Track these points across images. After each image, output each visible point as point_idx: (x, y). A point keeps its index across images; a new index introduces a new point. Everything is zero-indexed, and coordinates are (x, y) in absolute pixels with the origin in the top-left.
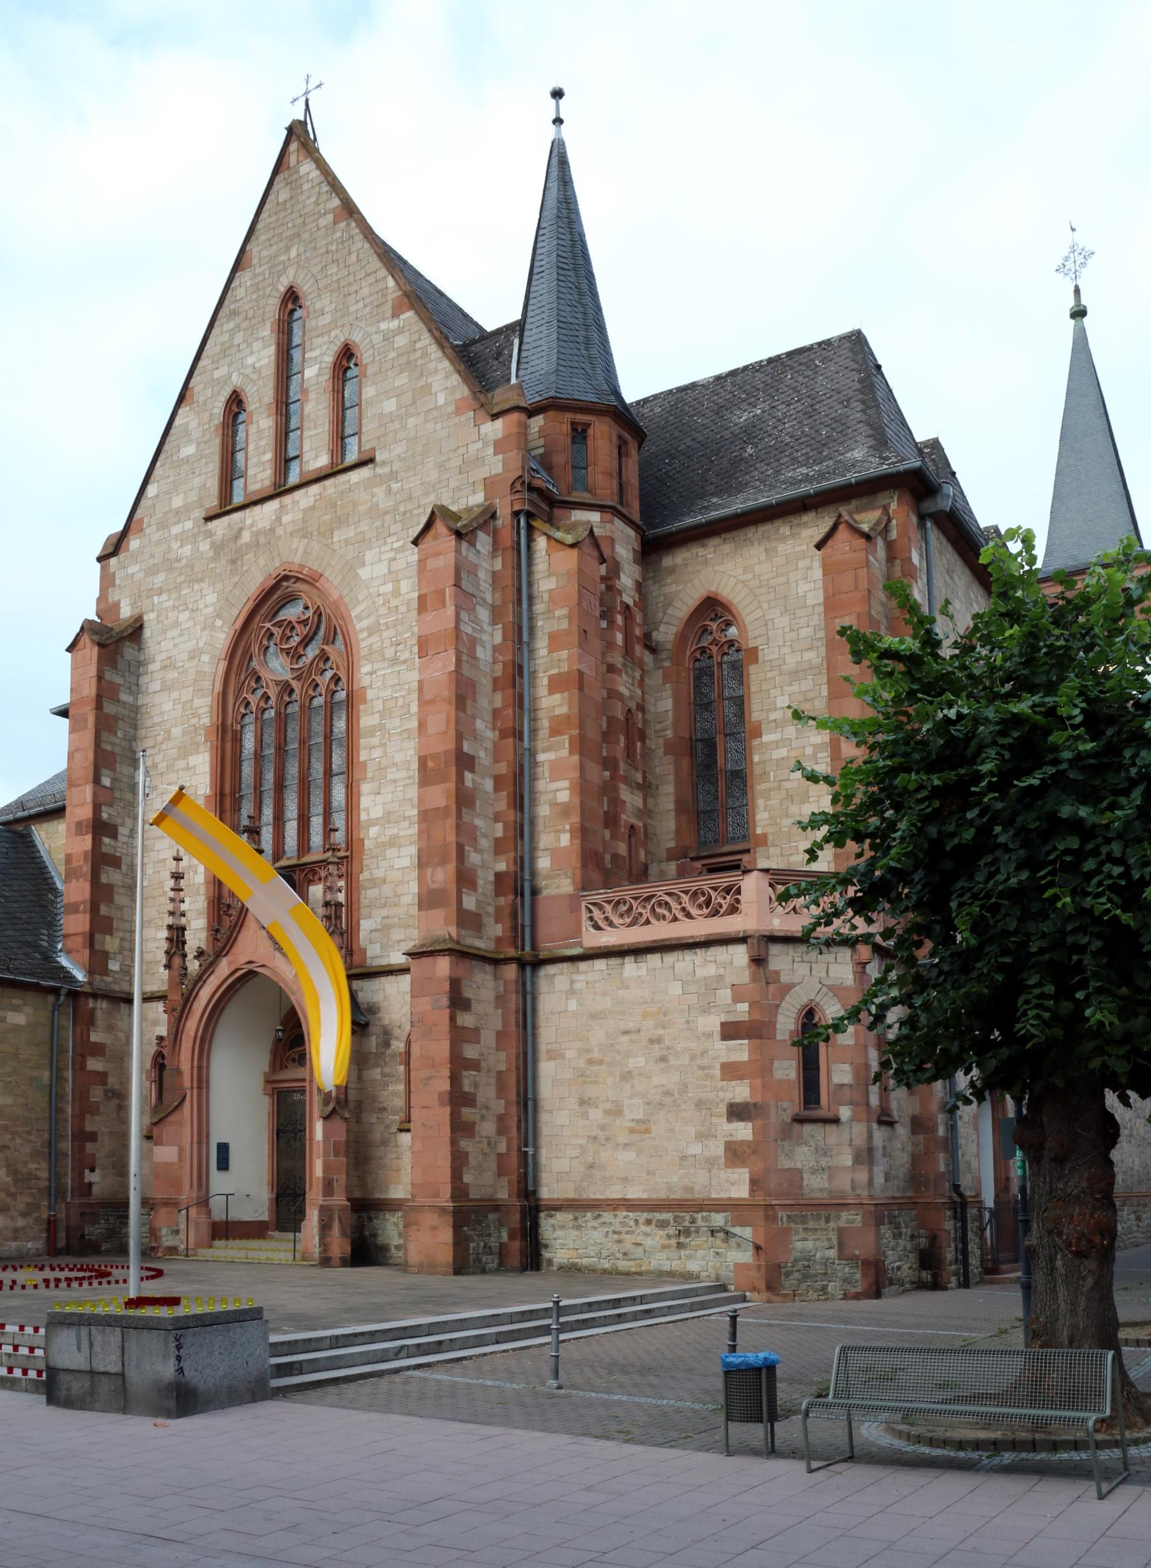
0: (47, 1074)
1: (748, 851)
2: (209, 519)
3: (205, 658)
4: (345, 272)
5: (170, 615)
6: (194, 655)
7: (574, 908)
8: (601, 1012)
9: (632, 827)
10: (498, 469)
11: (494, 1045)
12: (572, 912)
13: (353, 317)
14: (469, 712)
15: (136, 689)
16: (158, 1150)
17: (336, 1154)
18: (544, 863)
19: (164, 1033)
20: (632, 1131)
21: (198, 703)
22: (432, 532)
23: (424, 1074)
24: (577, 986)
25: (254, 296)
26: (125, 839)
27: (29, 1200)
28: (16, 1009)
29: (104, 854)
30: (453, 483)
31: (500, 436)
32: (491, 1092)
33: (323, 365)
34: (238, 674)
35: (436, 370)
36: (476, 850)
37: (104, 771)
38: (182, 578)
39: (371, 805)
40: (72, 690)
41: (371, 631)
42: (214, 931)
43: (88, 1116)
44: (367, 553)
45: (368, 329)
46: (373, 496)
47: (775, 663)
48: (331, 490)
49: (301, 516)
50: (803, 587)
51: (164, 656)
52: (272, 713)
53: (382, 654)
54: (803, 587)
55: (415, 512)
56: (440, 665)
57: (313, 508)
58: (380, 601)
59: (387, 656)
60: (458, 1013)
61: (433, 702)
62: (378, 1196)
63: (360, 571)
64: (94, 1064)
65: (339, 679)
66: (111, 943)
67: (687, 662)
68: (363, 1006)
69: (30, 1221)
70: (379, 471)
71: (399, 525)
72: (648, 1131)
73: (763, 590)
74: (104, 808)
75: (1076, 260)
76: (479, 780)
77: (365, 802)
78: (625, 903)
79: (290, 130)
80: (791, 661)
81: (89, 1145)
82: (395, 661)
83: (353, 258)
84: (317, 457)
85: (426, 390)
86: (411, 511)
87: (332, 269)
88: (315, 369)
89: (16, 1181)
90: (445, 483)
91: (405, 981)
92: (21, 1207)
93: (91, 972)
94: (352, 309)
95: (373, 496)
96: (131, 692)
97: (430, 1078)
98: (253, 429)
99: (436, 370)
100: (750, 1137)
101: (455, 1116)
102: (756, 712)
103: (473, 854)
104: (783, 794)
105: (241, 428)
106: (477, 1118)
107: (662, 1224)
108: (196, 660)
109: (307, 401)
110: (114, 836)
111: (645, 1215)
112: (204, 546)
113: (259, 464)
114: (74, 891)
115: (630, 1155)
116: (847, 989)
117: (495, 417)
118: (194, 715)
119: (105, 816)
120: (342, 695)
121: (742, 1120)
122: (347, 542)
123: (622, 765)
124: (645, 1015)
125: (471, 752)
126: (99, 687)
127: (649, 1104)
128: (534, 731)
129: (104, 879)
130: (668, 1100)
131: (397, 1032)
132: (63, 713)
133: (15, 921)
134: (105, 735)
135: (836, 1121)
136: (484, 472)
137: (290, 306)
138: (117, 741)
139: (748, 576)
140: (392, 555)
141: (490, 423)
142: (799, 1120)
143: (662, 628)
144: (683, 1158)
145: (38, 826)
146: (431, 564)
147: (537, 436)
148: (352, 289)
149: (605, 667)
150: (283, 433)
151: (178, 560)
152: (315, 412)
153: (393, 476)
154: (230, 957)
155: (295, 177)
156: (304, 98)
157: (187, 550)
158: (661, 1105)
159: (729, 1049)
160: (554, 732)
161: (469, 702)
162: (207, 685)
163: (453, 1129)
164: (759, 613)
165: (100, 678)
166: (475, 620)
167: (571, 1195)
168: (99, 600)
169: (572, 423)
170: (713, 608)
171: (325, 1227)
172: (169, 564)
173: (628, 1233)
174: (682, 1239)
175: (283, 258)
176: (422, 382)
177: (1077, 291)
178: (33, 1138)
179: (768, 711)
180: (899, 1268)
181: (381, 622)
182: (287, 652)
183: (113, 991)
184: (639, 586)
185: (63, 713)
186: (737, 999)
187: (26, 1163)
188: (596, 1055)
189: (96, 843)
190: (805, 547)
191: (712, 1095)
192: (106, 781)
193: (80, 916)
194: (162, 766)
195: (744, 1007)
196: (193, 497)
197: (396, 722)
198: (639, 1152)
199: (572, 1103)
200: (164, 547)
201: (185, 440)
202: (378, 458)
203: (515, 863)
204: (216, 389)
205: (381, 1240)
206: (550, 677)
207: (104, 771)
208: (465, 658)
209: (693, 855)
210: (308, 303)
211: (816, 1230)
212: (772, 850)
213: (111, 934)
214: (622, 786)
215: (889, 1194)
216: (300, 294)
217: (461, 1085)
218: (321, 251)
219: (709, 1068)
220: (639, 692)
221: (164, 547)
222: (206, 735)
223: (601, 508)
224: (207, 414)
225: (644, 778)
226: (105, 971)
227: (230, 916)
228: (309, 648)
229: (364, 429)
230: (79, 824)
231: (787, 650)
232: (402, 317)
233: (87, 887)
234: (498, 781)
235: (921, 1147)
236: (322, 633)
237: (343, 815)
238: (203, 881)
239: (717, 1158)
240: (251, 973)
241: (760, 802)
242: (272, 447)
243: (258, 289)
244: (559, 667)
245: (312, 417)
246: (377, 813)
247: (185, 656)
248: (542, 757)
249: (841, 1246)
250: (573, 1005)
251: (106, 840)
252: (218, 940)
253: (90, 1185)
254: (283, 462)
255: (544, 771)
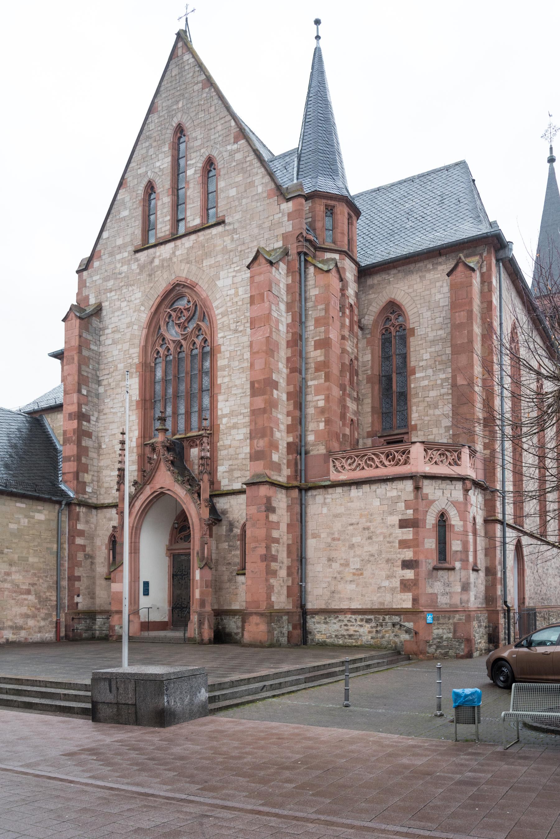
0: (55, 546)
1: (407, 433)
2: (136, 252)
3: (136, 327)
4: (208, 117)
5: (116, 303)
6: (130, 325)
7: (326, 461)
8: (339, 514)
9: (352, 420)
10: (290, 229)
11: (286, 531)
12: (325, 463)
13: (212, 142)
14: (276, 358)
15: (99, 343)
16: (113, 585)
17: (207, 587)
18: (311, 438)
19: (116, 525)
20: (354, 574)
21: (132, 351)
22: (258, 262)
23: (253, 545)
24: (327, 501)
25: (159, 128)
26: (94, 423)
27: (47, 612)
28: (39, 512)
29: (83, 430)
30: (266, 236)
31: (291, 210)
32: (285, 554)
33: (197, 168)
34: (153, 336)
35: (257, 173)
36: (279, 431)
37: (83, 387)
38: (123, 284)
39: (224, 406)
40: (65, 342)
41: (224, 314)
42: (142, 471)
43: (76, 568)
44: (221, 273)
45: (221, 149)
46: (224, 242)
47: (423, 336)
48: (202, 238)
49: (186, 251)
50: (438, 296)
51: (113, 325)
52: (171, 357)
53: (229, 327)
54: (438, 296)
55: (246, 251)
56: (261, 333)
57: (192, 247)
58: (228, 299)
59: (232, 328)
60: (270, 514)
61: (258, 352)
62: (226, 608)
63: (217, 282)
64: (79, 541)
65: (206, 340)
66: (87, 478)
67: (379, 336)
68: (219, 511)
69: (47, 622)
70: (227, 228)
71: (238, 258)
72: (362, 574)
73: (417, 298)
74: (83, 406)
75: (550, 133)
76: (280, 394)
77: (220, 405)
78: (351, 458)
79: (178, 34)
80: (431, 335)
81: (76, 583)
82: (236, 331)
83: (213, 109)
84: (194, 219)
85: (251, 184)
86: (244, 250)
87: (201, 115)
88: (193, 171)
89: (40, 602)
90: (262, 236)
91: (243, 497)
92: (42, 615)
93: (77, 492)
94: (212, 137)
95: (224, 242)
96: (96, 345)
97: (256, 547)
98: (159, 203)
99: (257, 173)
100: (413, 578)
101: (268, 566)
102: (413, 362)
103: (277, 433)
104: (426, 404)
105: (153, 202)
106: (278, 568)
107: (368, 621)
108: (131, 328)
109: (189, 188)
110: (89, 421)
111: (360, 617)
112: (134, 266)
113: (164, 222)
114: (66, 450)
115: (353, 586)
116: (460, 503)
117: (288, 200)
118: (130, 358)
119: (84, 410)
120: (208, 349)
121: (409, 569)
122: (210, 266)
123: (348, 388)
124: (361, 516)
125: (276, 380)
126: (80, 341)
127: (362, 560)
128: (306, 369)
129: (84, 444)
130: (372, 559)
131: (236, 524)
132: (58, 355)
133: (37, 465)
134: (83, 367)
135: (453, 569)
136: (282, 230)
137: (179, 135)
138: (90, 371)
139: (411, 290)
140: (234, 274)
141: (285, 204)
142: (436, 569)
143: (366, 317)
144: (379, 588)
145: (46, 415)
146: (257, 279)
147: (308, 211)
148: (212, 126)
149: (340, 338)
150: (177, 204)
151: (120, 274)
152: (193, 194)
153: (235, 231)
154: (151, 485)
155: (181, 62)
156: (185, 18)
157: (125, 268)
158: (369, 561)
159: (403, 533)
160: (317, 370)
161: (276, 353)
162: (137, 341)
163: (267, 574)
164: (415, 310)
165: (80, 336)
166: (278, 310)
167: (323, 607)
168: (78, 294)
169: (326, 205)
170: (393, 308)
171: (201, 623)
172: (115, 275)
173: (351, 626)
174: (379, 629)
175: (175, 107)
176: (249, 180)
177: (551, 148)
178: (48, 579)
179: (419, 361)
180: (480, 642)
181: (229, 310)
182: (179, 325)
183: (88, 503)
184: (357, 295)
185: (58, 355)
186: (407, 508)
187: (45, 592)
188: (336, 536)
189: (80, 425)
190: (439, 275)
191: (394, 556)
192: (84, 392)
193: (71, 463)
194: (113, 385)
195: (410, 512)
196: (128, 239)
197: (236, 363)
198: (357, 585)
199: (324, 560)
200: (113, 266)
201: (123, 207)
202: (227, 221)
203: (297, 438)
204: (139, 180)
205: (227, 630)
206: (315, 341)
207: (83, 387)
208: (274, 330)
209: (379, 435)
210: (189, 133)
211: (443, 624)
212: (419, 432)
213: (87, 473)
214: (348, 399)
215: (476, 606)
216: (185, 128)
217: (271, 551)
218: (195, 104)
219: (393, 542)
220: (356, 350)
221: (113, 266)
222: (136, 368)
223: (340, 252)
224: (135, 194)
225: (358, 395)
226: (85, 492)
227: (151, 464)
228: (190, 323)
229: (219, 205)
230: (70, 414)
231: (430, 329)
232: (239, 143)
233: (75, 448)
234: (289, 394)
235: (490, 582)
236: (197, 313)
237: (208, 412)
238: (135, 445)
239: (396, 588)
240: (162, 493)
241: (414, 408)
242: (170, 213)
243: (161, 125)
244: (319, 336)
245: (191, 197)
246: (226, 411)
247: (124, 326)
248: (310, 383)
249: (455, 632)
250: (325, 510)
251: (85, 423)
252: (144, 476)
253: (77, 603)
254: (176, 221)
255: (312, 390)
